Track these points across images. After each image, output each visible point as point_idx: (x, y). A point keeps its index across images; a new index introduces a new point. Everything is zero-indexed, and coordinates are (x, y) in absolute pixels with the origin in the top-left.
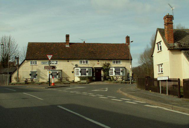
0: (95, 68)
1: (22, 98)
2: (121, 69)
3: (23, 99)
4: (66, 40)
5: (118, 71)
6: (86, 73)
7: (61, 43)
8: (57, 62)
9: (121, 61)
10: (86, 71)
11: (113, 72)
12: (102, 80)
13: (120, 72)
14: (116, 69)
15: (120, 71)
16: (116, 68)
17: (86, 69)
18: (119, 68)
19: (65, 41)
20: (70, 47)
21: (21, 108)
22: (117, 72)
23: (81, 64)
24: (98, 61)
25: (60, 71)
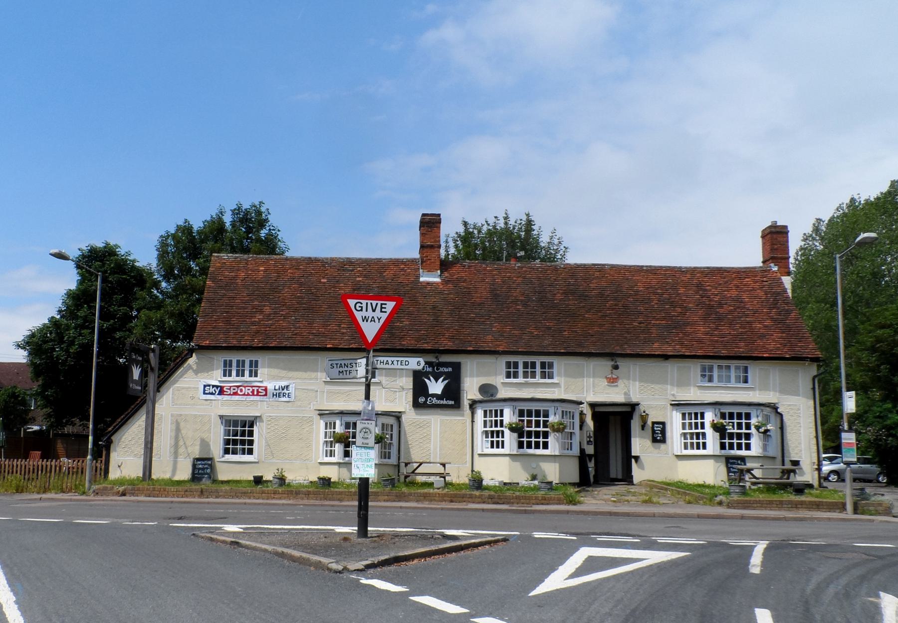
0: (593, 406)
1: (228, 518)
2: (753, 414)
3: (225, 518)
4: (422, 247)
5: (538, 424)
6: (546, 435)
7: (396, 262)
8: (746, 370)
9: (262, 358)
10: (545, 422)
11: (708, 430)
12: (613, 475)
13: (748, 436)
14: (521, 413)
15: (748, 427)
16: (526, 407)
17: (546, 415)
18: (699, 410)
19: (413, 252)
20: (445, 282)
21: (325, 557)
22: (529, 434)
23: (512, 380)
24: (616, 367)
25: (391, 421)
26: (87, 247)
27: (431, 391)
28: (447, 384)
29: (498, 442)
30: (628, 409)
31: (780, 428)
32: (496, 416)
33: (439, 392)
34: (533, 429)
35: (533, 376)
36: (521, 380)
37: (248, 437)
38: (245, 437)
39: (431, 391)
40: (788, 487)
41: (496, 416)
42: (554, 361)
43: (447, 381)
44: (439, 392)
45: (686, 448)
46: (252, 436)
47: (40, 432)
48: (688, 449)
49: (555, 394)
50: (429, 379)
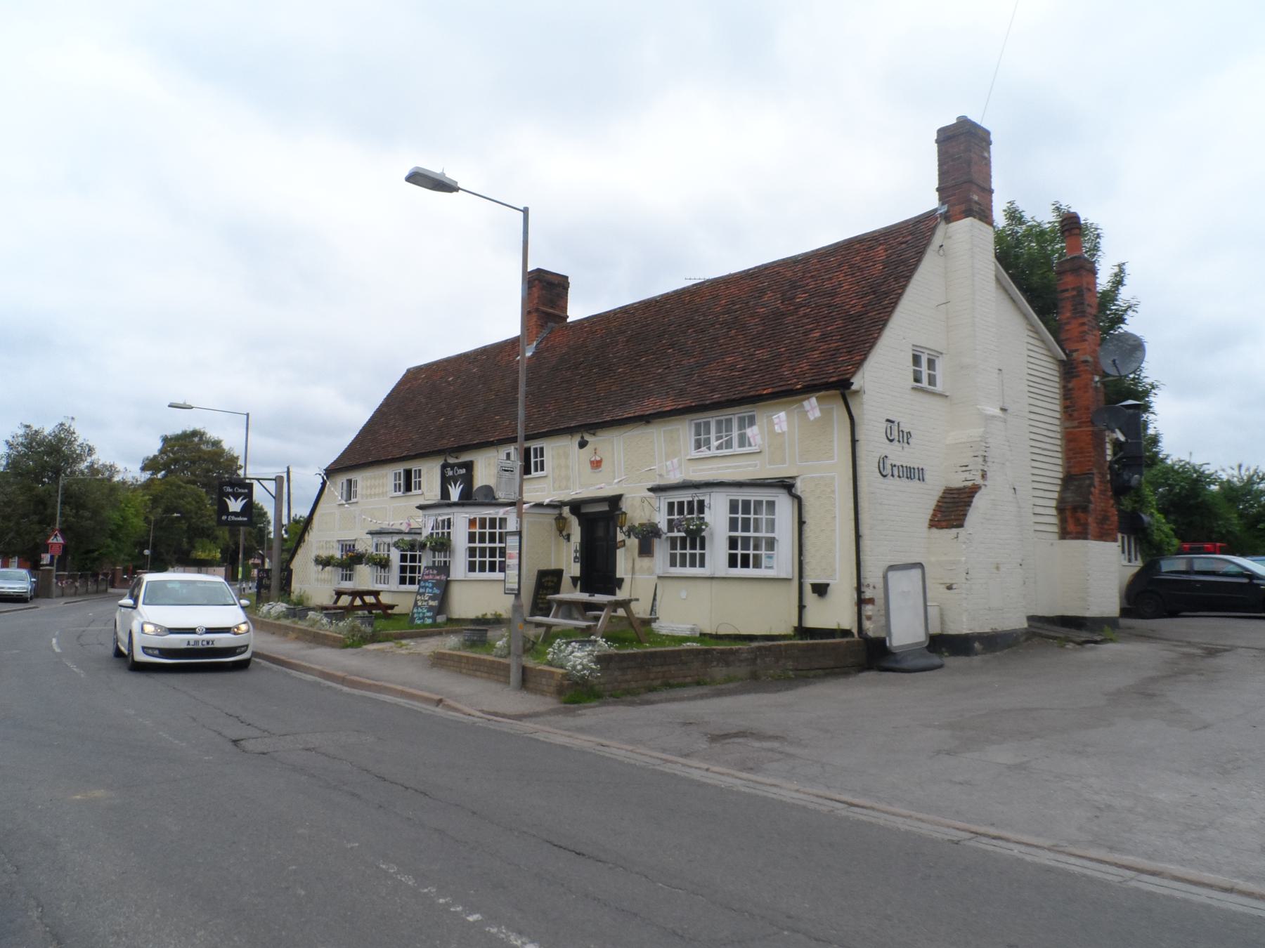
26: (1053, 205)
27: (231, 510)
28: (244, 505)
29: (693, 556)
30: (604, 508)
31: (804, 522)
32: (443, 528)
33: (239, 510)
34: (487, 545)
35: (729, 444)
36: (735, 449)
37: (410, 562)
38: (416, 562)
39: (231, 510)
40: (1106, 628)
41: (443, 528)
42: (358, 479)
43: (245, 501)
44: (239, 510)
45: (673, 564)
46: (401, 566)
47: (221, 553)
48: (695, 566)
49: (554, 491)
50: (230, 499)
